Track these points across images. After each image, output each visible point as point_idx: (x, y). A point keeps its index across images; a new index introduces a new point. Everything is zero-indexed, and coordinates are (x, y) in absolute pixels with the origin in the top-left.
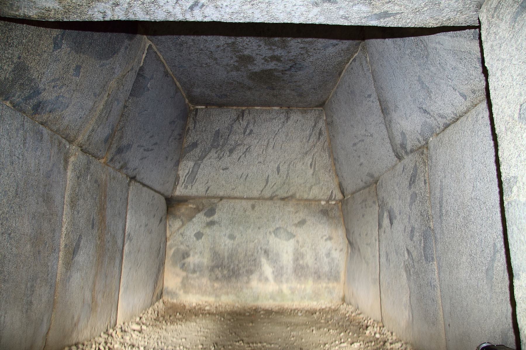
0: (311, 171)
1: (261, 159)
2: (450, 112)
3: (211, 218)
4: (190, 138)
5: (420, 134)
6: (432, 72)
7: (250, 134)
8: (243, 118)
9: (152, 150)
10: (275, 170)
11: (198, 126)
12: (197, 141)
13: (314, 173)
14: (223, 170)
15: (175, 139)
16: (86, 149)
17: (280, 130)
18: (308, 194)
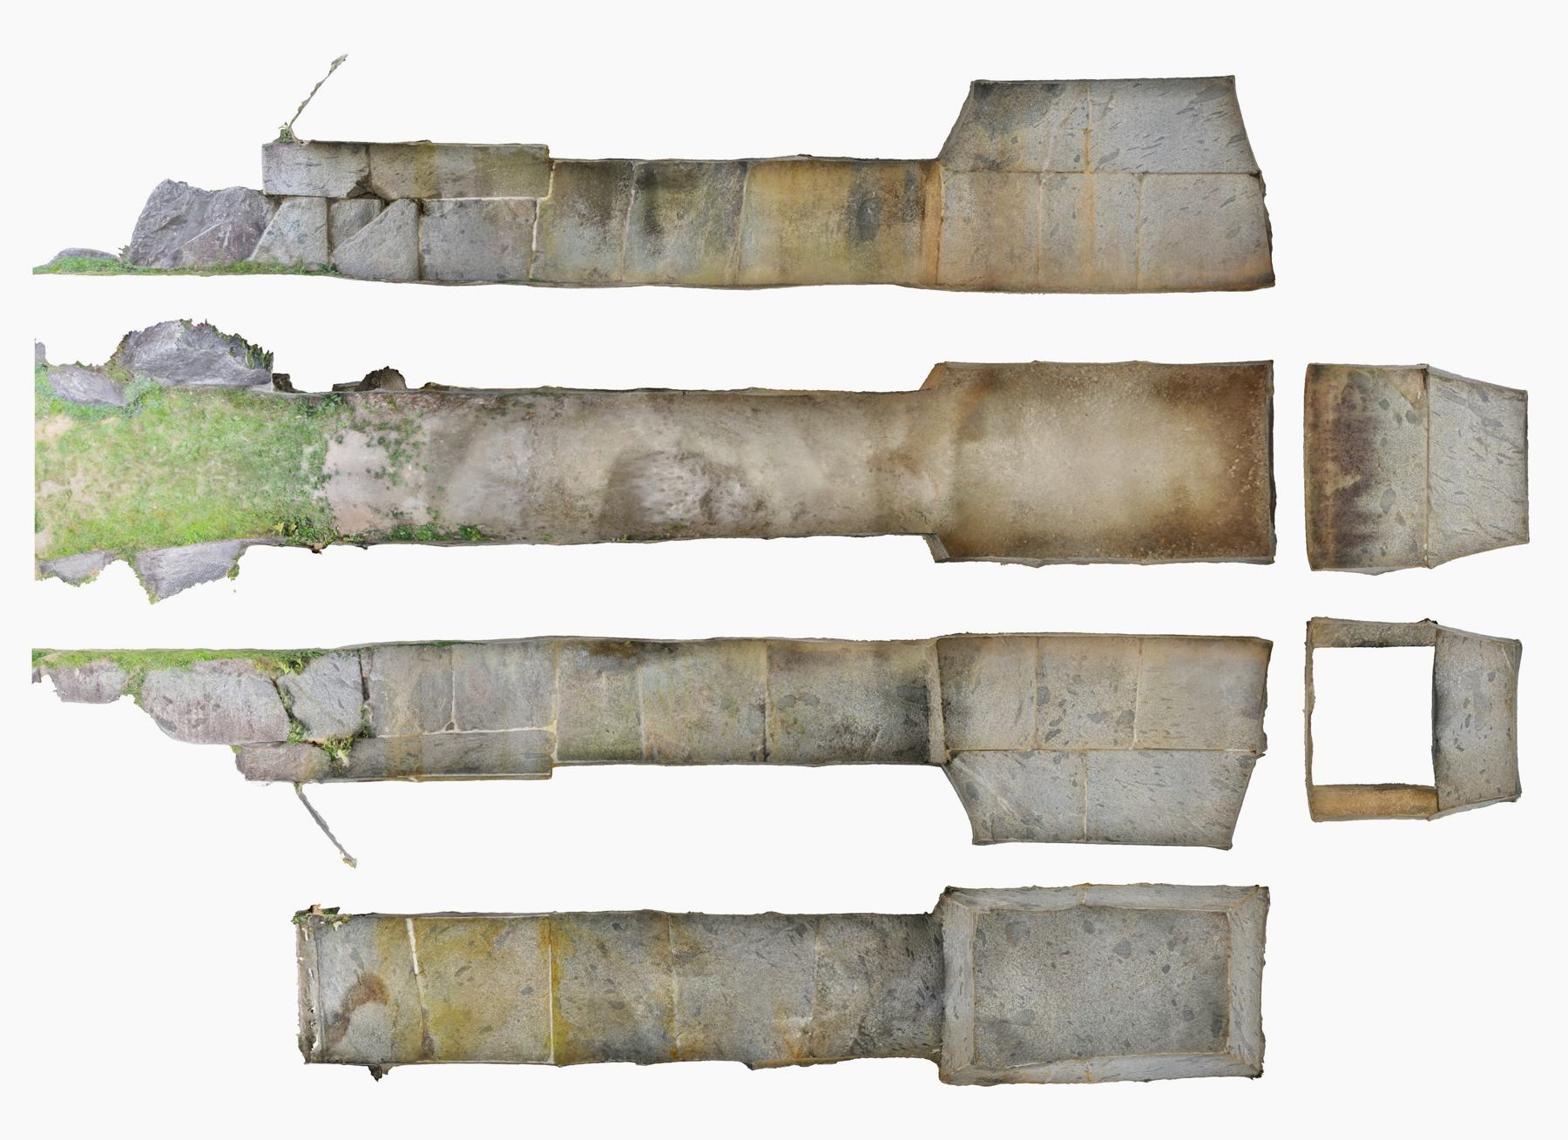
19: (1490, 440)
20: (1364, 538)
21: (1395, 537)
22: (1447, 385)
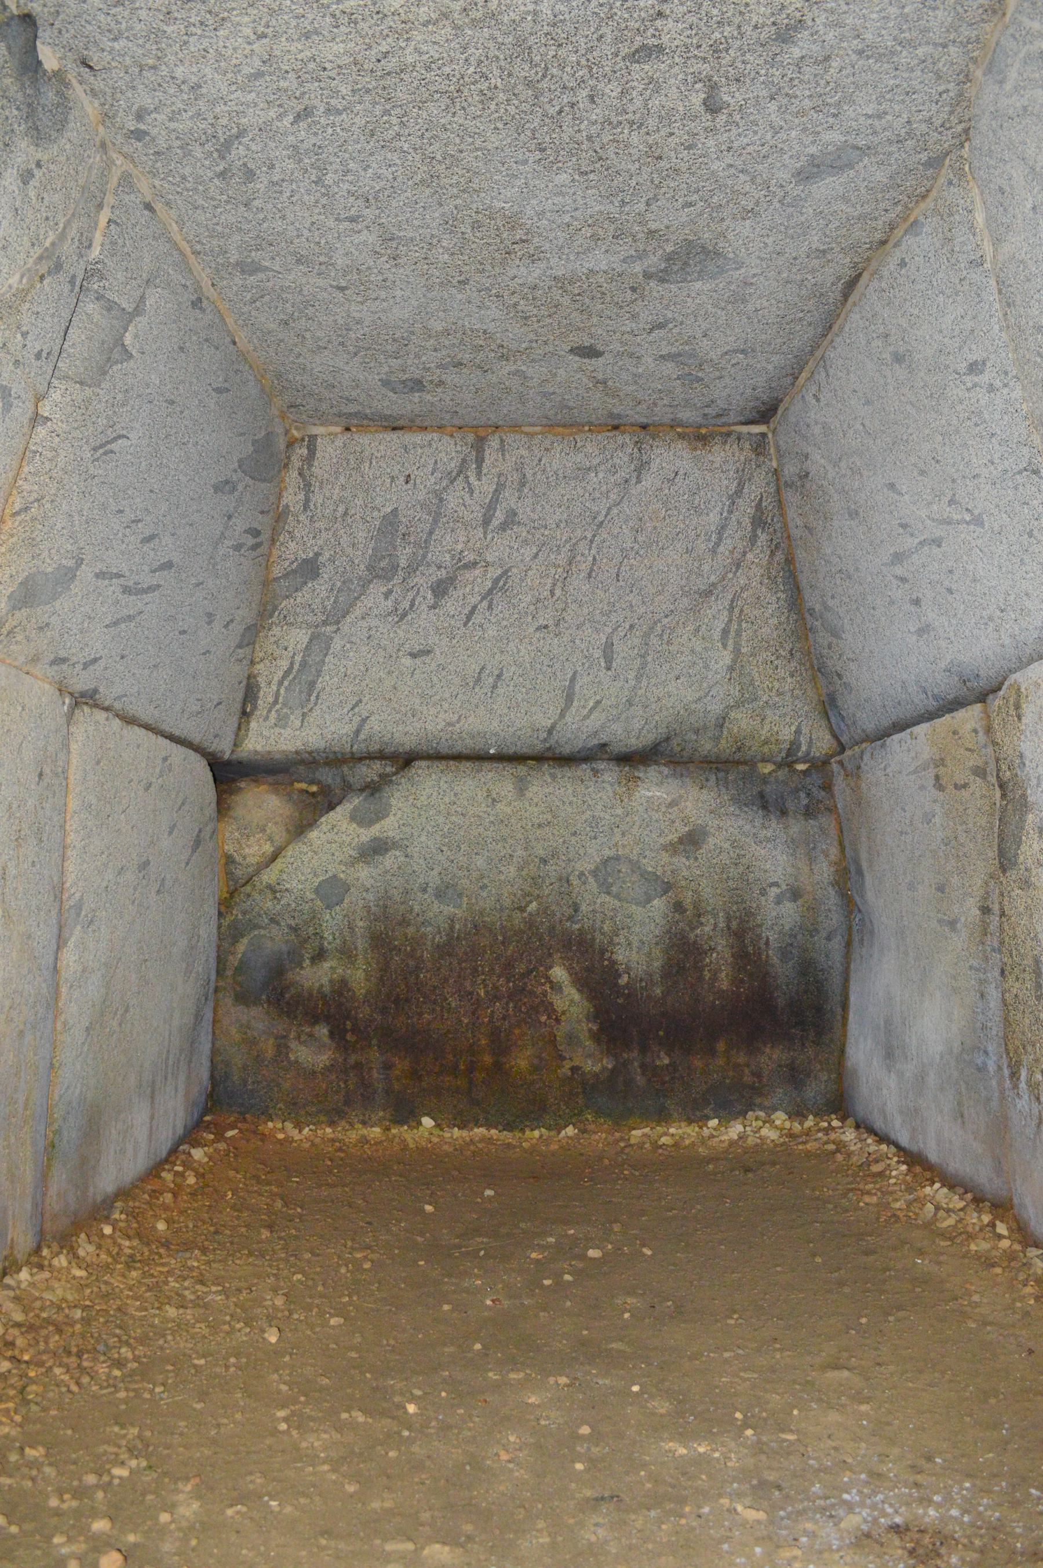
0: (726, 657)
3: (375, 830)
4: (292, 545)
7: (504, 527)
8: (479, 467)
9: (151, 589)
10: (597, 654)
11: (317, 498)
14: (414, 656)
15: (238, 547)
17: (615, 511)
18: (717, 739)
19: (441, 553)
20: (747, 953)
21: (768, 862)
22: (266, 695)
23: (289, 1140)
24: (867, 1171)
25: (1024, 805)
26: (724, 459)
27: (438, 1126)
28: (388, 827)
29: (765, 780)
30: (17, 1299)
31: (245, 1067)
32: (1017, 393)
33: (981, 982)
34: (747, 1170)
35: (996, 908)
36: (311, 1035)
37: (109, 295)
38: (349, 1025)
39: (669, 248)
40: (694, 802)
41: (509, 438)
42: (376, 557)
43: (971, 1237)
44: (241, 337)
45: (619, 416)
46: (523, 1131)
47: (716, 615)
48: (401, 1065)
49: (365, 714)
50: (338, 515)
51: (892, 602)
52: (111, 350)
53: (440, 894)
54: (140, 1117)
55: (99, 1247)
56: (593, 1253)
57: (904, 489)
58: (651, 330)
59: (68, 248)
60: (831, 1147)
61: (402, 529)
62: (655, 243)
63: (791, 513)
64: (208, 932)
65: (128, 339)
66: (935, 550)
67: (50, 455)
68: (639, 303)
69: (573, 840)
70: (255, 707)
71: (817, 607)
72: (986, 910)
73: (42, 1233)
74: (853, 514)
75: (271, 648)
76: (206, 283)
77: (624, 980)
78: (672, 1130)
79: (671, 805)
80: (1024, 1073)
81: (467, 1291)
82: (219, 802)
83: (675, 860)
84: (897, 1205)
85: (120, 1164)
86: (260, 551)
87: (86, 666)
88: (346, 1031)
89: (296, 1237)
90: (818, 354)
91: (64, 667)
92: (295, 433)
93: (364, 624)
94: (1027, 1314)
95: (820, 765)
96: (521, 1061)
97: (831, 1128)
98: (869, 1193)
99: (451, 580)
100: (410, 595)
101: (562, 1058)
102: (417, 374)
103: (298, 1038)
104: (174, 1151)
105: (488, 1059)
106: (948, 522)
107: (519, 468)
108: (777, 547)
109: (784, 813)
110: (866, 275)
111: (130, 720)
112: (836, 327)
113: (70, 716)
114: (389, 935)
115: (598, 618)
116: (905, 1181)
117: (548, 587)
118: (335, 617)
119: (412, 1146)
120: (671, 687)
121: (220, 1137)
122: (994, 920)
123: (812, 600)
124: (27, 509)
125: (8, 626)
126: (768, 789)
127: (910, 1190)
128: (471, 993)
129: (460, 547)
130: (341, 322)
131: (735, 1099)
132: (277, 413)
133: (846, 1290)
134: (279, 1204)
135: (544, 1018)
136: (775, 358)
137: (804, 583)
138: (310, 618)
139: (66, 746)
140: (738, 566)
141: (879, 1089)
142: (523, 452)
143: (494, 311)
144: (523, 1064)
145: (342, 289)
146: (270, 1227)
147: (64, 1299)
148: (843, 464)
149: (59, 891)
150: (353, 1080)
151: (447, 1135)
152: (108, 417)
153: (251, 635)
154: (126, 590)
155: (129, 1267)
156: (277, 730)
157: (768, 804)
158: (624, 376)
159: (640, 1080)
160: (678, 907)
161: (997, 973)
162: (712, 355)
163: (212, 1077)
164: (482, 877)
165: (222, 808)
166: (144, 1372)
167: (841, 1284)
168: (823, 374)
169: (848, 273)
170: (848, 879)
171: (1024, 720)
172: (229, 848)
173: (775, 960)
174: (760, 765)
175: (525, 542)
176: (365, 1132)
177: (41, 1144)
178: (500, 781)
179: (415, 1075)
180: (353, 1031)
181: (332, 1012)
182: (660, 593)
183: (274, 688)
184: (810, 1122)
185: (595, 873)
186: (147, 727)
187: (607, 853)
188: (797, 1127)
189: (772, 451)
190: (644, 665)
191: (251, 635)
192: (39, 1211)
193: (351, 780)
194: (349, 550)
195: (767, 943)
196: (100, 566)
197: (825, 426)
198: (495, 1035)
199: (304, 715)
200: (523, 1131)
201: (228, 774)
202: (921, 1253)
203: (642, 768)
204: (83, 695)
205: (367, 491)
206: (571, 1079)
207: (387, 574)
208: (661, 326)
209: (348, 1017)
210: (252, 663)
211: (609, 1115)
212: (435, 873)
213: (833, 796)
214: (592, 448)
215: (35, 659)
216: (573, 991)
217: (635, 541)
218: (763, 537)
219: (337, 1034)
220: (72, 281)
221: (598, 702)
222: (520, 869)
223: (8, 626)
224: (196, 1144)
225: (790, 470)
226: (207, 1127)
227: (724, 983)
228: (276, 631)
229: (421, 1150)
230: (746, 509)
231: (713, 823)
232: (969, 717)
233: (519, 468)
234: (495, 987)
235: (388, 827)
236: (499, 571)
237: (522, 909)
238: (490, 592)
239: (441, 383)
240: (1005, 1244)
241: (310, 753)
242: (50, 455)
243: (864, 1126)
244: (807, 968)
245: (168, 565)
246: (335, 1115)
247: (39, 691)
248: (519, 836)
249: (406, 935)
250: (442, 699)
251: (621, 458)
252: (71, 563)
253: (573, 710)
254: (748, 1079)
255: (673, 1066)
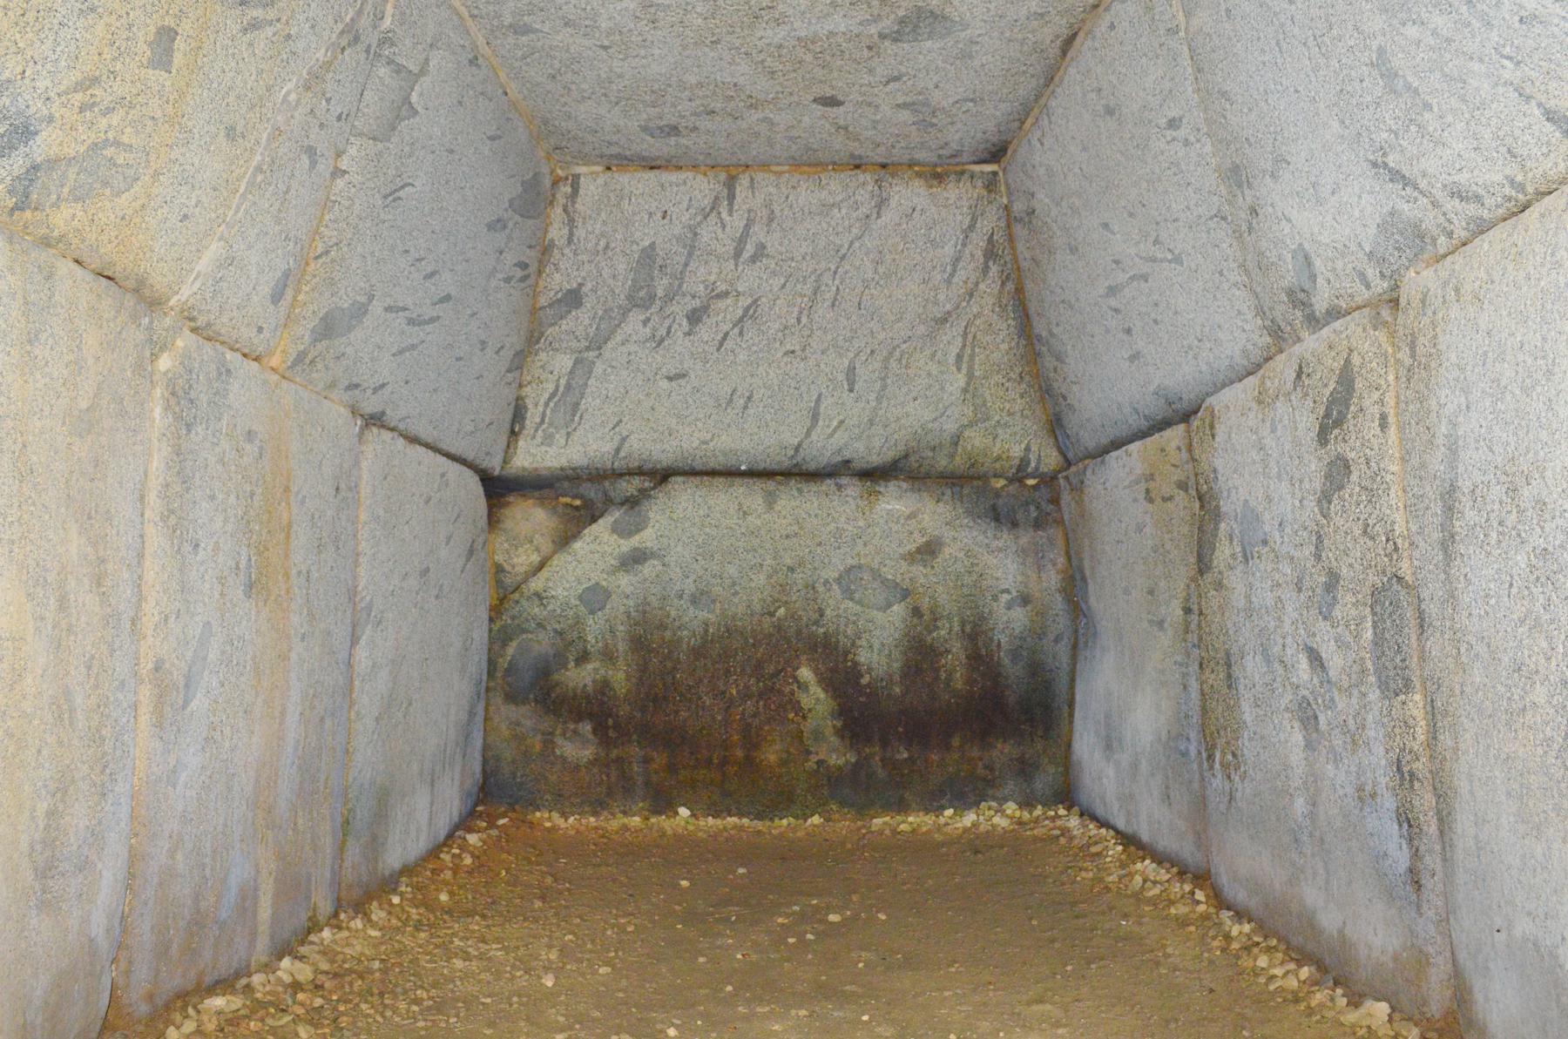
0: (961, 380)
1: (793, 343)
2: (1499, 178)
3: (635, 541)
4: (557, 276)
5: (1370, 255)
6: (1434, 33)
7: (753, 259)
8: (731, 204)
9: (433, 320)
10: (841, 377)
11: (580, 233)
12: (581, 285)
13: (968, 384)
14: (670, 379)
15: (508, 280)
16: (209, 325)
17: (857, 244)
18: (952, 456)
21: (999, 572)
23: (554, 829)
24: (1087, 852)
25: (1217, 515)
26: (958, 196)
27: (693, 815)
28: (646, 538)
29: (997, 494)
30: (323, 953)
31: (514, 762)
32: (1208, 148)
33: (1184, 675)
34: (977, 852)
35: (1195, 608)
36: (575, 731)
37: (399, 60)
38: (610, 722)
39: (901, 13)
40: (931, 514)
41: (759, 176)
42: (636, 287)
43: (1172, 903)
44: (513, 88)
45: (860, 157)
46: (772, 820)
47: (951, 341)
48: (660, 759)
49: (625, 433)
50: (600, 248)
51: (1108, 331)
52: (400, 108)
53: (694, 601)
54: (422, 801)
55: (390, 913)
56: (833, 918)
57: (1116, 228)
58: (888, 83)
59: (365, 22)
60: (1057, 832)
61: (659, 261)
62: (888, 9)
63: (1020, 246)
64: (480, 635)
65: (414, 98)
66: (1143, 284)
67: (347, 203)
68: (876, 59)
69: (819, 550)
70: (522, 428)
71: (1044, 334)
72: (1188, 611)
73: (339, 899)
74: (1073, 250)
75: (537, 372)
76: (481, 41)
77: (865, 680)
78: (911, 819)
79: (909, 517)
80: (1218, 755)
81: (719, 947)
82: (490, 515)
83: (913, 568)
84: (1111, 879)
85: (406, 842)
86: (528, 282)
87: (375, 391)
88: (608, 728)
89: (567, 907)
90: (1042, 101)
91: (357, 392)
92: (560, 172)
93: (624, 349)
94: (1211, 962)
95: (1049, 480)
96: (771, 755)
97: (1058, 817)
98: (1086, 870)
99: (705, 309)
100: (667, 323)
101: (808, 753)
102: (673, 121)
103: (564, 734)
104: (450, 836)
105: (739, 753)
106: (1154, 260)
107: (768, 205)
108: (1007, 278)
109: (1015, 525)
110: (1081, 34)
111: (413, 440)
112: (1056, 79)
113: (361, 435)
114: (647, 639)
115: (841, 343)
116: (1120, 860)
117: (795, 315)
118: (597, 343)
119: (670, 832)
120: (910, 408)
121: (492, 825)
122: (1194, 618)
123: (1040, 327)
124: (327, 252)
125: (310, 357)
126: (1000, 502)
127: (1123, 866)
128: (724, 693)
129: (713, 278)
130: (604, 76)
131: (967, 792)
132: (543, 154)
133: (1057, 945)
134: (549, 880)
135: (791, 716)
136: (1002, 106)
137: (1032, 311)
138: (574, 344)
139: (357, 463)
140: (971, 295)
141: (1100, 779)
142: (771, 189)
143: (744, 67)
144: (772, 758)
145: (605, 48)
146: (543, 898)
147: (362, 954)
148: (1064, 204)
149: (352, 593)
150: (614, 774)
151: (702, 823)
152: (397, 168)
153: (520, 361)
154: (411, 322)
155: (417, 929)
156: (544, 448)
157: (999, 516)
158: (864, 122)
159: (881, 773)
160: (916, 612)
161: (1197, 667)
162: (944, 103)
163: (484, 771)
164: (734, 584)
165: (493, 521)
166: (439, 1007)
167: (1053, 941)
168: (1046, 121)
169: (1066, 32)
170: (1074, 585)
171: (1217, 439)
172: (499, 558)
173: (1006, 661)
174: (993, 481)
175: (774, 273)
176: (626, 820)
177: (339, 820)
178: (750, 496)
179: (672, 768)
180: (614, 728)
181: (594, 710)
182: (899, 320)
183: (541, 409)
184: (1039, 811)
185: (838, 580)
186: (427, 446)
187: (850, 562)
188: (1026, 816)
189: (1003, 189)
190: (884, 387)
191: (520, 361)
192: (336, 882)
193: (612, 494)
194: (611, 281)
195: (999, 645)
196: (389, 301)
197: (1049, 169)
198: (746, 730)
199: (568, 434)
200: (772, 820)
201: (499, 489)
202: (1126, 916)
203: (882, 483)
204: (372, 417)
205: (627, 226)
206: (817, 771)
207: (645, 304)
208: (896, 79)
209: (610, 715)
210: (521, 386)
211: (852, 806)
212: (690, 580)
213: (1060, 510)
214: (835, 185)
215: (332, 385)
216: (819, 690)
217: (876, 272)
218: (994, 269)
219: (600, 729)
220: (368, 51)
221: (842, 422)
222: (770, 577)
223: (310, 357)
224: (470, 830)
225: (1019, 207)
226: (480, 815)
227: (959, 683)
228: (543, 355)
229: (677, 837)
230: (978, 242)
231: (948, 534)
232: (1174, 435)
233: (768, 205)
234: (747, 687)
235: (646, 538)
236: (749, 301)
237: (772, 614)
238: (741, 320)
239: (696, 128)
240: (1202, 908)
241: (574, 469)
242: (347, 203)
243: (1088, 814)
244: (1036, 669)
245: (447, 298)
246: (598, 806)
247: (336, 414)
248: (768, 546)
249: (663, 638)
250: (697, 419)
251: (863, 195)
252: (363, 299)
253: (818, 429)
254: (980, 771)
255: (911, 760)
